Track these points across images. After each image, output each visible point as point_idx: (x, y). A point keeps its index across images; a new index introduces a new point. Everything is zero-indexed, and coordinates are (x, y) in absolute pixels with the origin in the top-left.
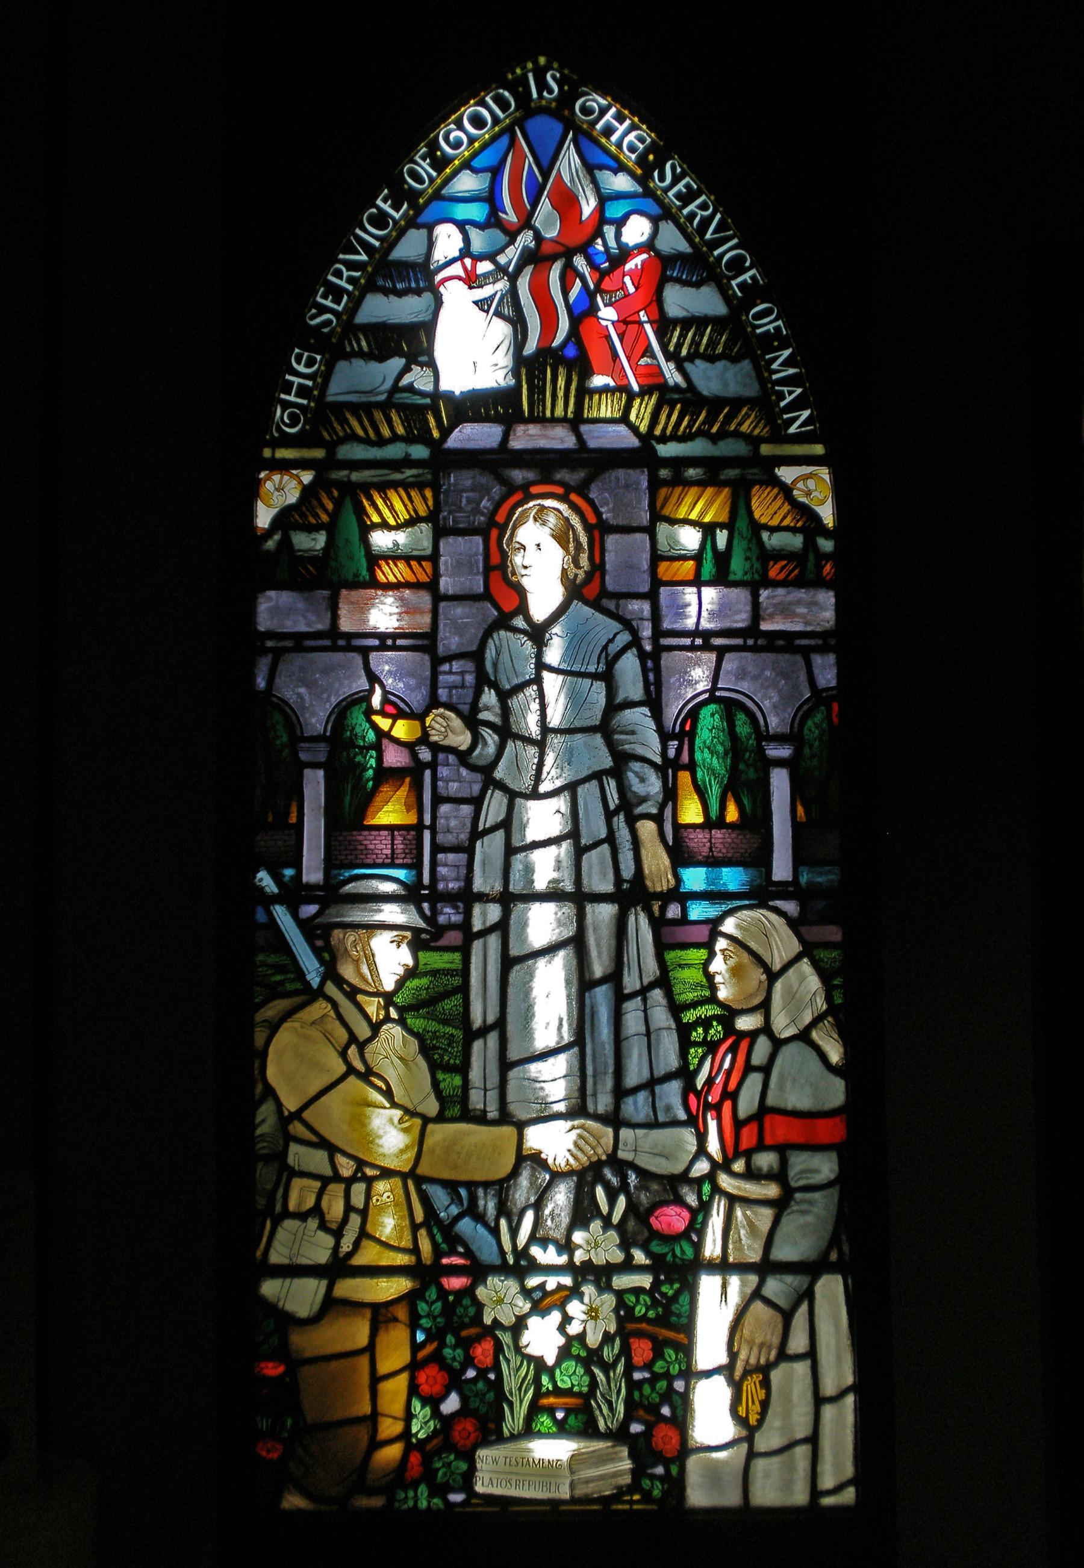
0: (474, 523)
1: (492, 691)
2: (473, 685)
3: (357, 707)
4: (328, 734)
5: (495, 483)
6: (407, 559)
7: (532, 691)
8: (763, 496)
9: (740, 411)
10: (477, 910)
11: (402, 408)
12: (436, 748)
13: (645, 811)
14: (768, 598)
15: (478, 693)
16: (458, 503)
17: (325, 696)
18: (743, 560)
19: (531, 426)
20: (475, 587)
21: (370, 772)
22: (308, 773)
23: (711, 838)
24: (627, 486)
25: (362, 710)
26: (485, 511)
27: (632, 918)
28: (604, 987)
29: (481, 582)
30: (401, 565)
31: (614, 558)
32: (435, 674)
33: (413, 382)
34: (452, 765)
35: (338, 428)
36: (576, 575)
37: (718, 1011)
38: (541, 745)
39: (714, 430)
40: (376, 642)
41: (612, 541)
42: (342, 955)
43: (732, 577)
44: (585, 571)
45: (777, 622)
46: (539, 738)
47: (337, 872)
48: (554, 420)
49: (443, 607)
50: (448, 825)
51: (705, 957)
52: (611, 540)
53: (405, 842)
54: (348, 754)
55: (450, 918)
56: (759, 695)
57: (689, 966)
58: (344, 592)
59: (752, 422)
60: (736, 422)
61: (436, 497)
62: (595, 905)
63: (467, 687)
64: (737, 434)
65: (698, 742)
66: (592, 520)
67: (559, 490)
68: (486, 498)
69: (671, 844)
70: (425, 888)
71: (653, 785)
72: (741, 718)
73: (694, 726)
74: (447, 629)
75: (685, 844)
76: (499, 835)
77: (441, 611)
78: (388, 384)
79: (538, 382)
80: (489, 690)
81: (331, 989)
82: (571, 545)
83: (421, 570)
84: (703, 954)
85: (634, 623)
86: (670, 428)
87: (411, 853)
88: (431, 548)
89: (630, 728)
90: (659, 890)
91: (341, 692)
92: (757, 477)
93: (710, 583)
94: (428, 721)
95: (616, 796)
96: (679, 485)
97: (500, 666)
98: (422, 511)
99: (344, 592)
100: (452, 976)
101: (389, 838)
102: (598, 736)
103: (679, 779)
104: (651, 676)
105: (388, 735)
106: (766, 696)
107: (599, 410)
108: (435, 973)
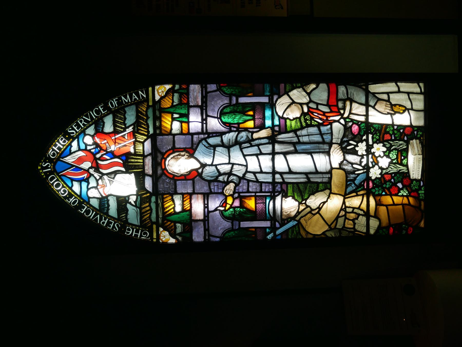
0: (173, 184)
1: (219, 178)
4: (231, 221)
5: (161, 178)
6: (183, 201)
7: (219, 167)
8: (164, 104)
9: (140, 111)
10: (277, 181)
11: (141, 204)
12: (234, 192)
13: (251, 136)
14: (192, 103)
17: (221, 222)
19: (145, 169)
21: (241, 210)
26: (169, 180)
27: (279, 140)
28: (297, 147)
29: (189, 181)
30: (185, 203)
34: (239, 188)
35: (147, 221)
36: (187, 155)
37: (303, 117)
38: (233, 164)
39: (145, 118)
40: (206, 209)
41: (177, 146)
42: (289, 216)
43: (187, 113)
48: (144, 162)
51: (289, 120)
52: (177, 146)
53: (259, 200)
56: (219, 105)
57: (291, 125)
58: (193, 218)
59: (143, 107)
60: (143, 112)
62: (275, 149)
63: (218, 184)
64: (146, 112)
65: (232, 122)
66: (171, 151)
67: (163, 160)
68: (166, 180)
69: (259, 129)
70: (271, 194)
72: (225, 110)
76: (258, 175)
77: (197, 192)
81: (297, 218)
82: (179, 157)
83: (186, 198)
84: (288, 121)
85: (200, 139)
86: (145, 130)
88: (180, 195)
89: (228, 140)
90: (271, 132)
92: (159, 106)
93: (188, 118)
94: (227, 195)
95: (247, 144)
99: (193, 218)
101: (258, 204)
102: (230, 149)
103: (242, 127)
104: (214, 135)
105: (231, 205)
106: (219, 104)
107: (140, 150)
108: (293, 191)
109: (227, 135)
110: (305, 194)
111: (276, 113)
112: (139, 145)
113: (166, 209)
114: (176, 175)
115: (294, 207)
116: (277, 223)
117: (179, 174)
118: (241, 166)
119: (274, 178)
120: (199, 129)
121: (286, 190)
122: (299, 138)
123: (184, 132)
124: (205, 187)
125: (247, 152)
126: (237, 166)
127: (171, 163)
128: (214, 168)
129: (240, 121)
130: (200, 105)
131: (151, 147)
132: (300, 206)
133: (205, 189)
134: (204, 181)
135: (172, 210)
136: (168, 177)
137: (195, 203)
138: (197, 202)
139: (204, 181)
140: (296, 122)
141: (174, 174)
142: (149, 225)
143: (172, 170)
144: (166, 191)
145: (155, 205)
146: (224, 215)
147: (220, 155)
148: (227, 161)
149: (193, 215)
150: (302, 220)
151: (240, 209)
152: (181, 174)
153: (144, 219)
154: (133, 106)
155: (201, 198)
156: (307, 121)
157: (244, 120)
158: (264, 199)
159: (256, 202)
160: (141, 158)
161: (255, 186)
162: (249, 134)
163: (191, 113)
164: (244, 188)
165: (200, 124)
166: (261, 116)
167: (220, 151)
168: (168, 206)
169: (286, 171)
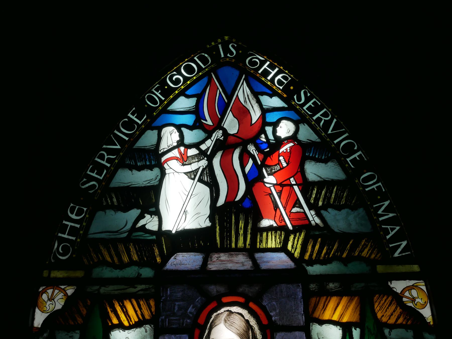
0: (183, 323)
9: (360, 243)
19: (222, 254)
26: (191, 315)
39: (344, 255)
48: (237, 250)
59: (369, 250)
61: (157, 305)
64: (360, 258)
67: (241, 300)
68: (192, 306)
86: (315, 255)
107: (267, 243)
112: (278, 240)
113: (120, 305)
114: (206, 334)
127: (236, 322)
135: (115, 321)
141: (208, 328)
142: (85, 261)
143: (217, 322)
153: (102, 248)
160: (247, 244)
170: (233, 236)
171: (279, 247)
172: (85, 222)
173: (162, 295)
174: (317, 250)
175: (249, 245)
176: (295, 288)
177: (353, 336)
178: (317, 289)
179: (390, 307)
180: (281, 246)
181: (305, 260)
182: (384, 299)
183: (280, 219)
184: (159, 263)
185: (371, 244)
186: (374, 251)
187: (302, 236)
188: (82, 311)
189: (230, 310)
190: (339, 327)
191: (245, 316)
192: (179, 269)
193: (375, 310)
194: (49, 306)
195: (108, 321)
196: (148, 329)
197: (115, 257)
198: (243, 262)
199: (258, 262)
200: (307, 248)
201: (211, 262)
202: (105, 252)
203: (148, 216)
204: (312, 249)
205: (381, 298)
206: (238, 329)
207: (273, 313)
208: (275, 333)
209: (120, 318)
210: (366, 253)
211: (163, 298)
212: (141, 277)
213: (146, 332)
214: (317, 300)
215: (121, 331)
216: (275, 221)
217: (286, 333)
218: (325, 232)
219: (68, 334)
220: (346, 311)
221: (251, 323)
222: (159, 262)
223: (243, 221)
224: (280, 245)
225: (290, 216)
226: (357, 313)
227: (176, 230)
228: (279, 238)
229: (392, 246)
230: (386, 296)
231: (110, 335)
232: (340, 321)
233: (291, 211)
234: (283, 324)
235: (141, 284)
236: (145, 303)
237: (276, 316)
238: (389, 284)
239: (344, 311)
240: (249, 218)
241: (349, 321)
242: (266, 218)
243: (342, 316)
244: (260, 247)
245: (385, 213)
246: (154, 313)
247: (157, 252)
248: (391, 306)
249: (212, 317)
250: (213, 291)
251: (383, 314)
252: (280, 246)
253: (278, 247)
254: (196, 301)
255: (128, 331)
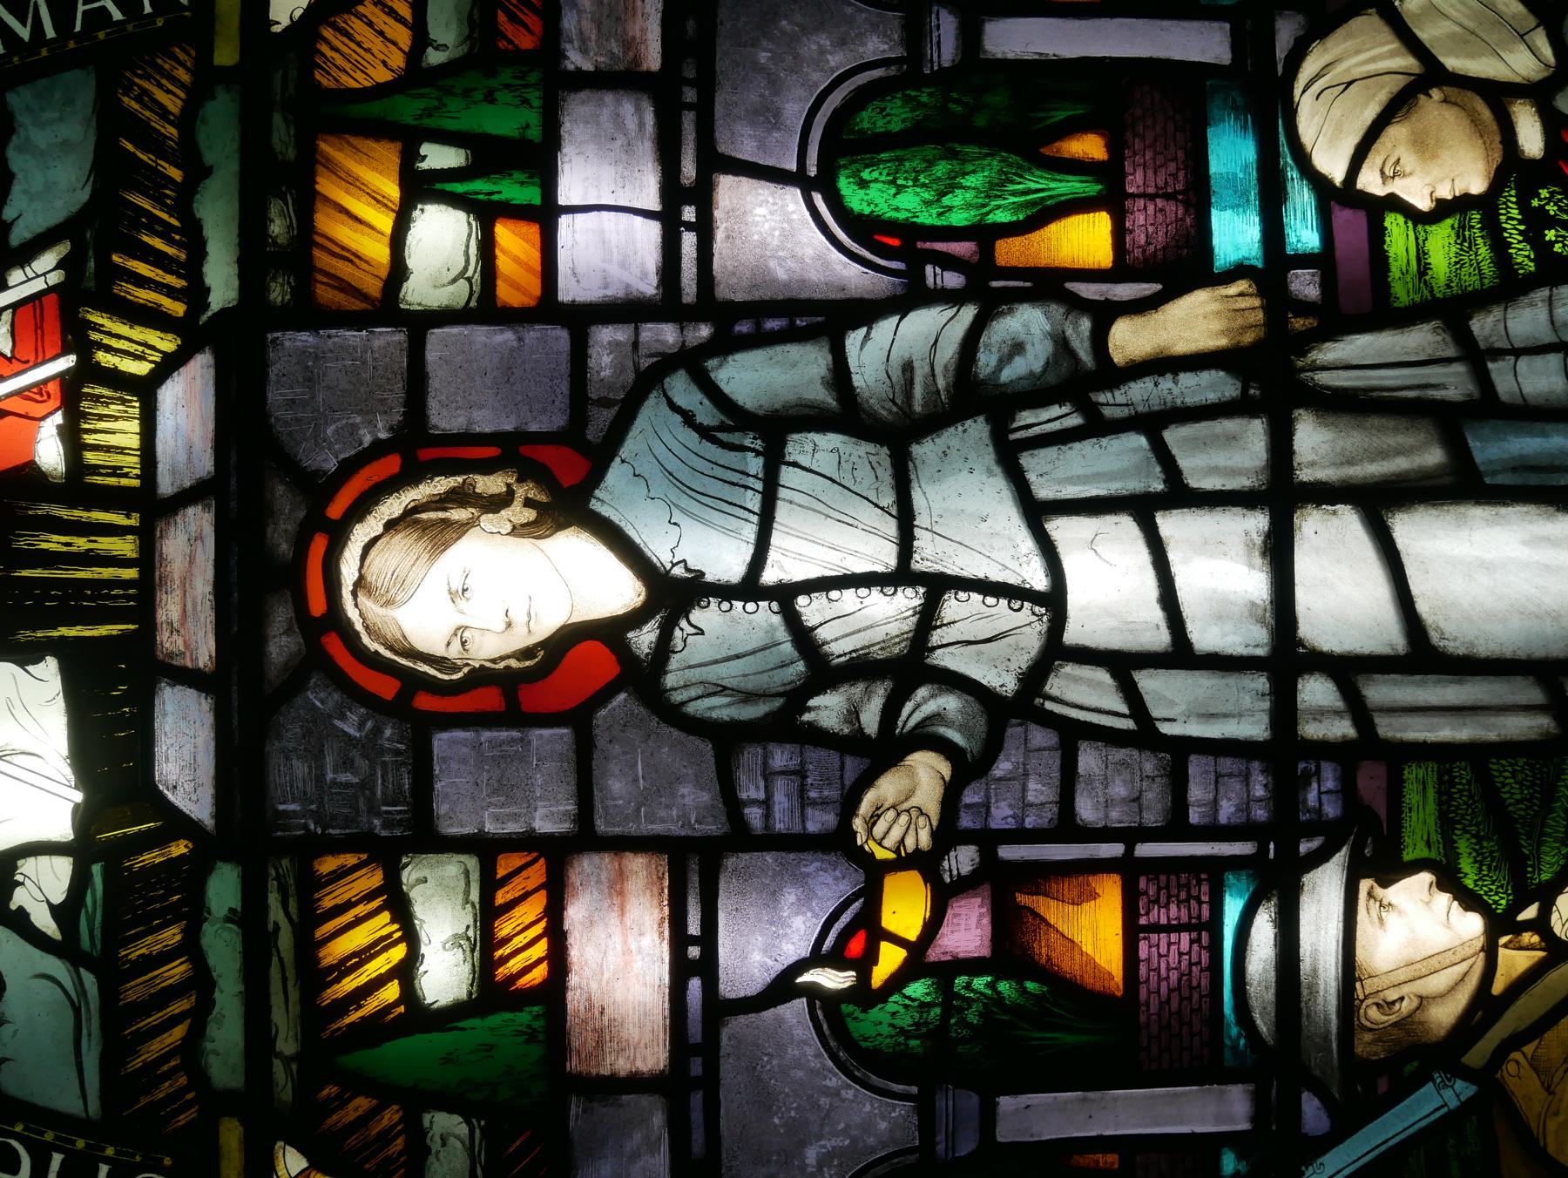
0: (397, 752)
1: (812, 703)
2: (798, 747)
3: (851, 1024)
4: (914, 1090)
5: (299, 701)
6: (489, 914)
7: (811, 609)
8: (339, 60)
9: (132, 115)
10: (1311, 730)
11: (116, 930)
12: (947, 834)
13: (1087, 344)
14: (584, 51)
15: (818, 737)
16: (350, 791)
17: (824, 1101)
18: (492, 107)
19: (161, 616)
20: (558, 747)
21: (1004, 987)
22: (1005, 1133)
23: (1144, 195)
24: (310, 381)
25: (858, 1013)
26: (369, 724)
27: (1324, 378)
28: (1473, 444)
29: (546, 732)
30: (505, 928)
31: (484, 412)
32: (772, 842)
33: (51, 906)
34: (988, 796)
35: (166, 1088)
36: (528, 503)
37: (1511, 195)
38: (938, 586)
39: (175, 174)
40: (695, 984)
41: (444, 417)
42: (1408, 1032)
43: (535, 134)
44: (519, 480)
45: (644, 31)
46: (921, 590)
47: (1227, 1054)
48: (148, 559)
49: (607, 823)
50: (1124, 801)
51: (1401, 219)
52: (444, 417)
53: (1163, 899)
54: (964, 1041)
55: (1329, 792)
56: (815, 76)
57: (1421, 254)
58: (573, 1065)
59: (160, 86)
60: (156, 123)
61: (337, 847)
62: (1297, 459)
63: (802, 764)
64: (188, 120)
65: (927, 218)
66: (391, 465)
67: (319, 545)
68: (337, 723)
69: (1159, 287)
70: (1263, 849)
71: (1026, 326)
72: (869, 120)
73: (893, 227)
74: (662, 813)
75: (1160, 255)
76: (1149, 682)
77: (617, 830)
78: (55, 966)
79: (53, 598)
80: (809, 709)
81: (1477, 1055)
82: (458, 514)
83: (516, 880)
84: (1395, 224)
85: (645, 363)
86: (171, 280)
87: (1188, 886)
88: (463, 858)
89: (896, 374)
90: (1260, 315)
91: (815, 1064)
92: (293, 74)
93: (548, 181)
94: (881, 854)
95: (1056, 411)
96: (310, 257)
97: (750, 685)
98: (372, 879)
99: (573, 1065)
100: (1452, 784)
101: (1154, 937)
102: (917, 450)
103: (1014, 263)
104: (772, 324)
105: (917, 950)
106: (819, 63)
107: (121, 450)
108: (1447, 824)
109: (884, 328)
110: (1545, 848)
111: (1295, 159)
112: (114, 409)
113: (338, 980)
114: (432, 672)
115: (1449, 957)
116: (1305, 1096)
117: (456, 669)
118: (1003, 602)
119: (1284, 709)
120: (644, 275)
121: (1382, 813)
122: (1490, 365)
123: (506, 294)
124: (685, 790)
125: (1061, 482)
126: (976, 597)
127: (392, 564)
128: (763, 617)
129: (998, 207)
130: (649, 73)
131: (211, 426)
132: (1502, 951)
133: (687, 800)
134: (676, 733)
135: (391, 992)
136: (357, 695)
137: (599, 931)
138: (613, 918)
139: (681, 729)
140: (1460, 232)
141: (411, 665)
142: (183, 1119)
143: (391, 632)
144: (334, 817)
145: (239, 947)
146: (855, 1035)
147: (821, 507)
148: (884, 557)
149: (580, 1039)
150: (1512, 1067)
151: (998, 978)
152: (474, 670)
153: (138, 1063)
154: (71, 76)
155: (650, 884)
156: (1550, 235)
157: (1033, 203)
158: (1205, 888)
159: (1138, 915)
160: (126, 522)
161: (1126, 775)
162: (1076, 326)
163: (576, 132)
164: (1031, 798)
165: (651, 232)
166: (1175, 176)
167: (825, 463)
168: (355, 954)
169: (1386, 651)
170: (96, 576)
171: (137, 404)
172: (42, 1134)
173: (302, 832)
174: (152, 269)
175: (128, 517)
176: (280, 354)
177: (446, 167)
178: (289, 278)
179: (355, 35)
180: (135, 399)
181: (186, 313)
182: (329, 53)
183: (37, 397)
184: (190, 845)
185: (140, 77)
186: (165, 70)
187: (100, 321)
188: (360, 1112)
189: (351, 588)
190: (416, 213)
191: (373, 535)
192: (212, 772)
193: (365, 88)
194: (639, 475)
195: (392, 1016)
196: (414, 876)
197: (169, 1010)
198: (189, 540)
199: (189, 484)
200: (145, 305)
201: (188, 654)
202: (152, 1048)
203: (20, 898)
204: (150, 289)
205: (325, 63)
206: (415, 558)
207: (365, 435)
208: (432, 432)
209: (381, 974)
210: (171, 96)
211: (312, 827)
212: (239, 909)
213: (426, 882)
214: (325, 280)
215: (422, 969)
216: (44, 418)
217: (432, 394)
218: (88, 235)
219: (434, 1151)
220: (363, 184)
221: (396, 515)
222: (186, 846)
223: (42, 537)
224: (131, 401)
225: (27, 362)
226: (373, 149)
227: (70, 787)
228: (108, 404)
229: (151, 5)
230: (318, 46)
231: (435, 1006)
232: (397, 209)
233: (9, 355)
234: (401, 400)
235: (265, 908)
236: (328, 889)
237: (376, 426)
238: (279, 30)
239: (364, 191)
240: (30, 513)
241: (397, 177)
242: (32, 451)
243: (381, 199)
244: (137, 477)
245: (30, 15)
246: (361, 856)
247: (151, 857)
248: (352, 32)
249: (376, 652)
250: (286, 646)
251: (380, 63)
252: (134, 404)
253: (137, 410)
254: (320, 709)
255: (422, 945)
